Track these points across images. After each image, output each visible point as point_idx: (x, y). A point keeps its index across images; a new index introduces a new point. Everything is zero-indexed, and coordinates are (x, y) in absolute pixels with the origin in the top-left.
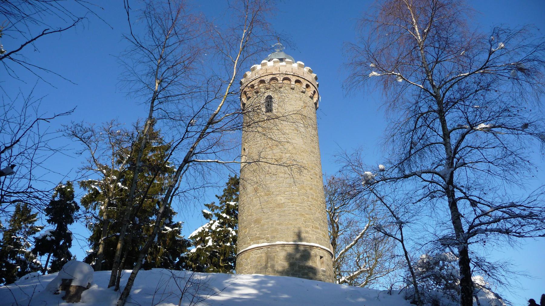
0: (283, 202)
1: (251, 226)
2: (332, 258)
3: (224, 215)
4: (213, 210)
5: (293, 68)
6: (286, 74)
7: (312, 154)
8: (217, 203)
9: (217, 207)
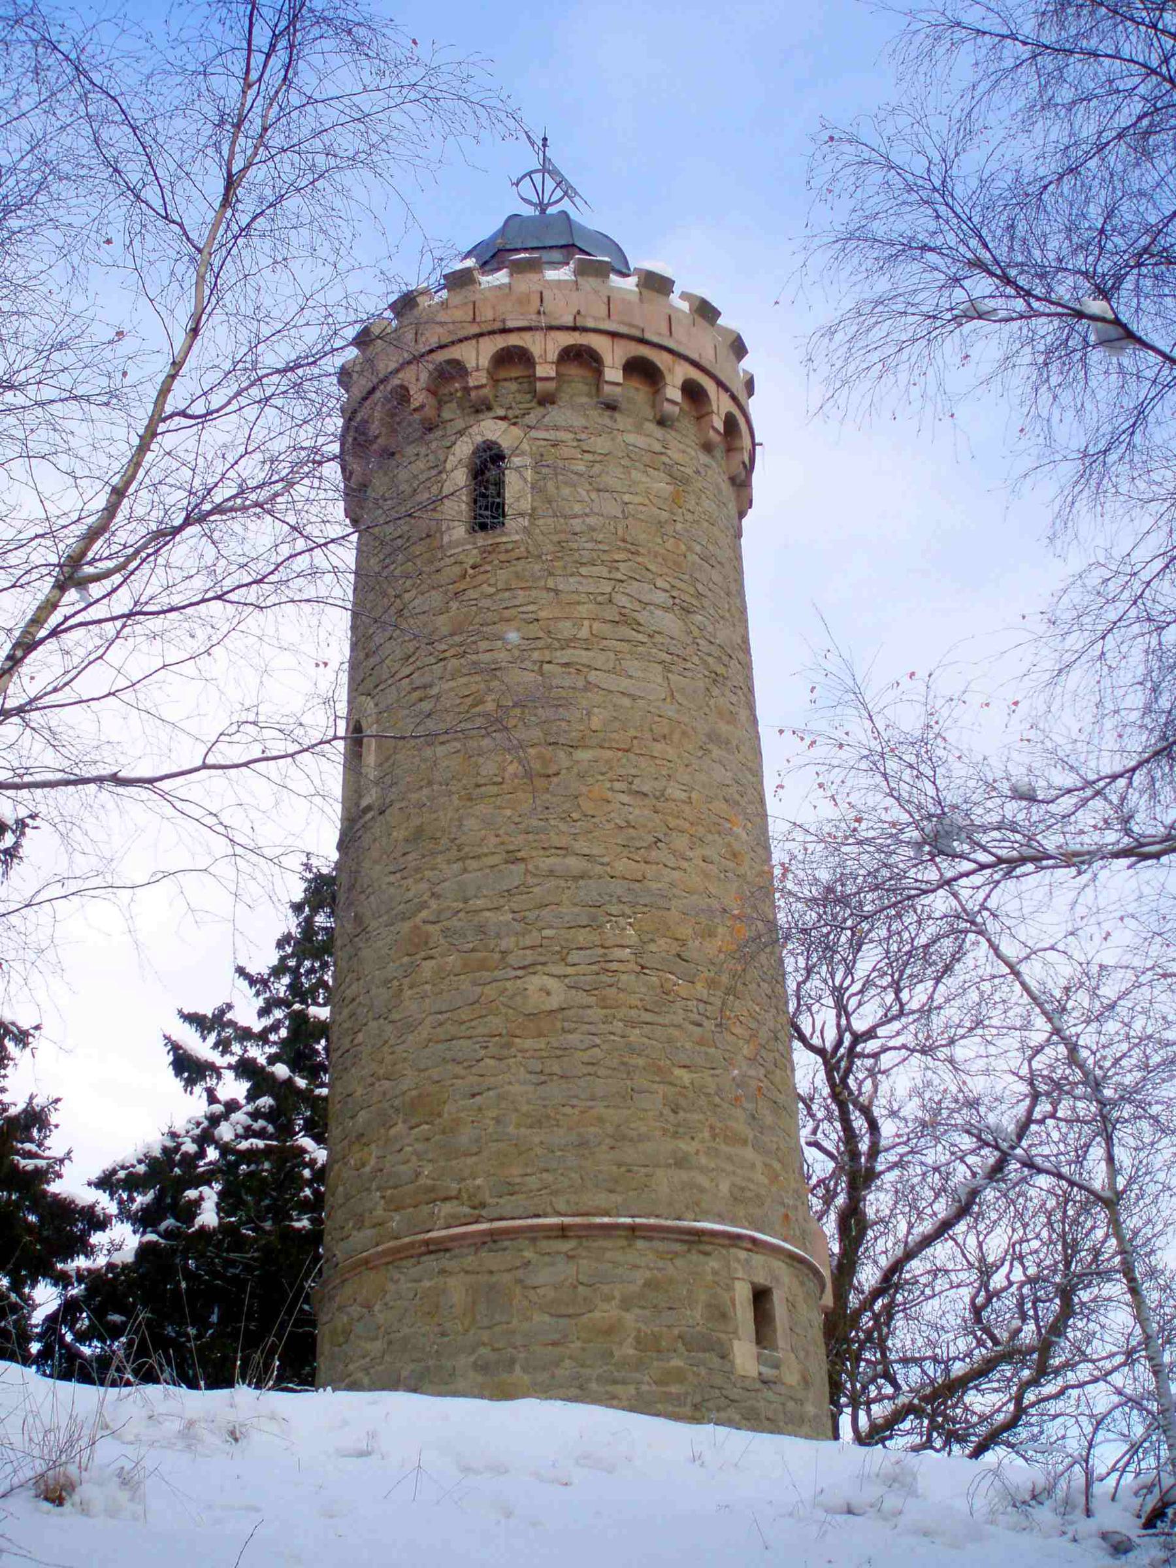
0: (555, 1006)
1: (393, 1132)
2: (822, 1291)
3: (281, 1070)
4: (223, 1046)
5: (614, 296)
6: (574, 329)
7: (716, 752)
8: (247, 1013)
9: (245, 1034)
